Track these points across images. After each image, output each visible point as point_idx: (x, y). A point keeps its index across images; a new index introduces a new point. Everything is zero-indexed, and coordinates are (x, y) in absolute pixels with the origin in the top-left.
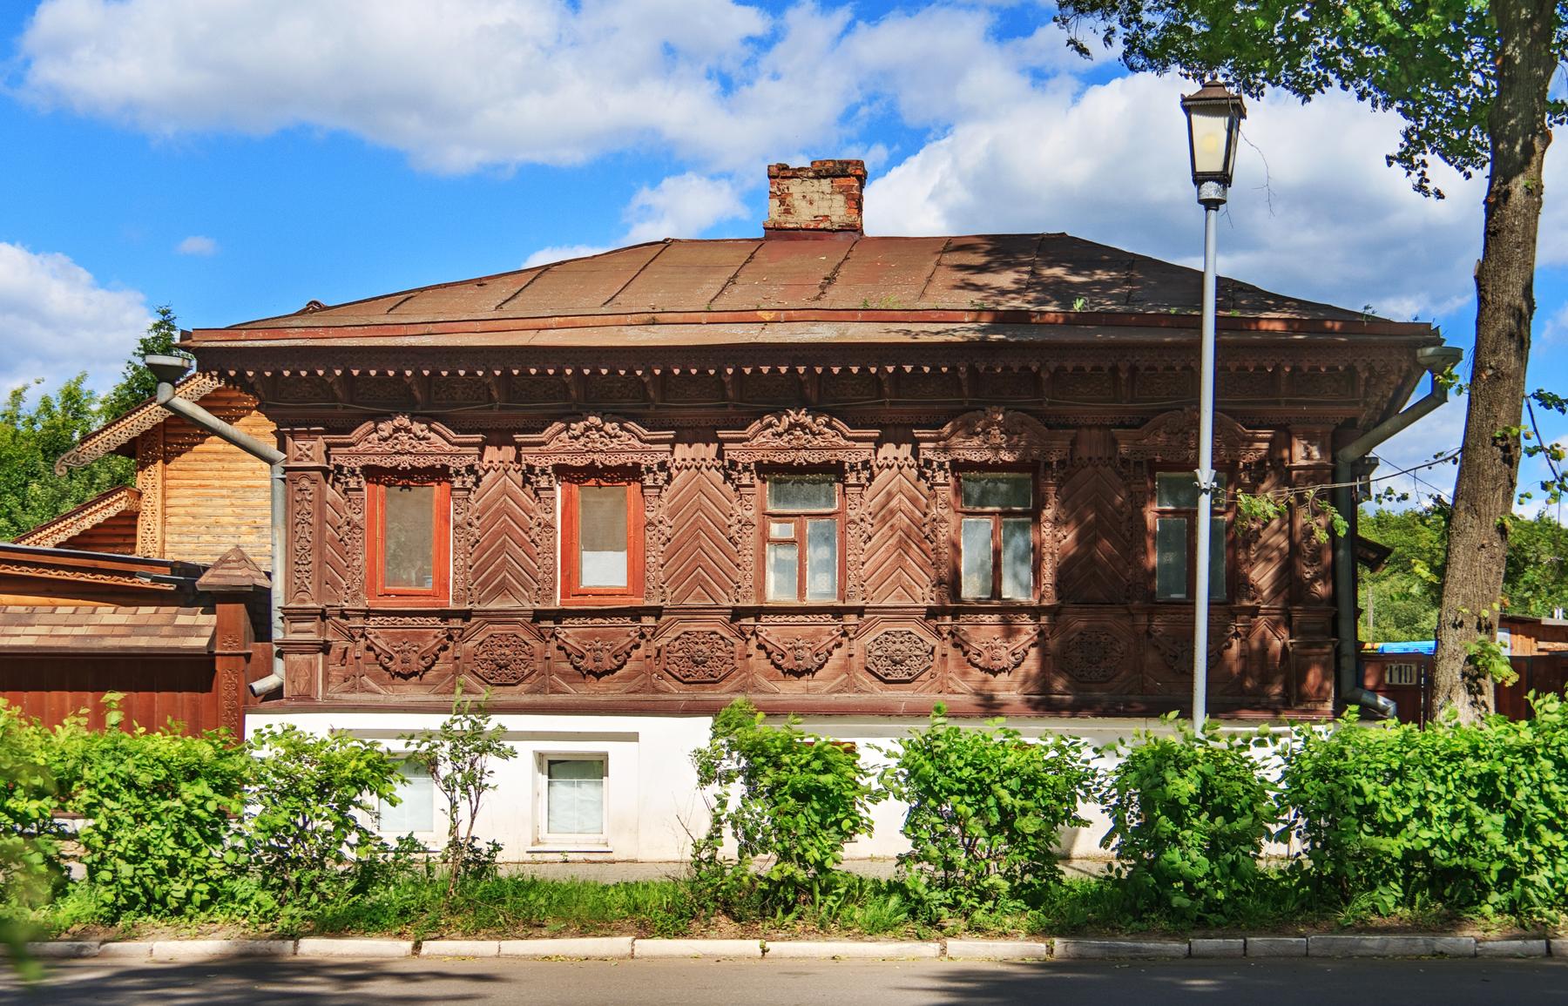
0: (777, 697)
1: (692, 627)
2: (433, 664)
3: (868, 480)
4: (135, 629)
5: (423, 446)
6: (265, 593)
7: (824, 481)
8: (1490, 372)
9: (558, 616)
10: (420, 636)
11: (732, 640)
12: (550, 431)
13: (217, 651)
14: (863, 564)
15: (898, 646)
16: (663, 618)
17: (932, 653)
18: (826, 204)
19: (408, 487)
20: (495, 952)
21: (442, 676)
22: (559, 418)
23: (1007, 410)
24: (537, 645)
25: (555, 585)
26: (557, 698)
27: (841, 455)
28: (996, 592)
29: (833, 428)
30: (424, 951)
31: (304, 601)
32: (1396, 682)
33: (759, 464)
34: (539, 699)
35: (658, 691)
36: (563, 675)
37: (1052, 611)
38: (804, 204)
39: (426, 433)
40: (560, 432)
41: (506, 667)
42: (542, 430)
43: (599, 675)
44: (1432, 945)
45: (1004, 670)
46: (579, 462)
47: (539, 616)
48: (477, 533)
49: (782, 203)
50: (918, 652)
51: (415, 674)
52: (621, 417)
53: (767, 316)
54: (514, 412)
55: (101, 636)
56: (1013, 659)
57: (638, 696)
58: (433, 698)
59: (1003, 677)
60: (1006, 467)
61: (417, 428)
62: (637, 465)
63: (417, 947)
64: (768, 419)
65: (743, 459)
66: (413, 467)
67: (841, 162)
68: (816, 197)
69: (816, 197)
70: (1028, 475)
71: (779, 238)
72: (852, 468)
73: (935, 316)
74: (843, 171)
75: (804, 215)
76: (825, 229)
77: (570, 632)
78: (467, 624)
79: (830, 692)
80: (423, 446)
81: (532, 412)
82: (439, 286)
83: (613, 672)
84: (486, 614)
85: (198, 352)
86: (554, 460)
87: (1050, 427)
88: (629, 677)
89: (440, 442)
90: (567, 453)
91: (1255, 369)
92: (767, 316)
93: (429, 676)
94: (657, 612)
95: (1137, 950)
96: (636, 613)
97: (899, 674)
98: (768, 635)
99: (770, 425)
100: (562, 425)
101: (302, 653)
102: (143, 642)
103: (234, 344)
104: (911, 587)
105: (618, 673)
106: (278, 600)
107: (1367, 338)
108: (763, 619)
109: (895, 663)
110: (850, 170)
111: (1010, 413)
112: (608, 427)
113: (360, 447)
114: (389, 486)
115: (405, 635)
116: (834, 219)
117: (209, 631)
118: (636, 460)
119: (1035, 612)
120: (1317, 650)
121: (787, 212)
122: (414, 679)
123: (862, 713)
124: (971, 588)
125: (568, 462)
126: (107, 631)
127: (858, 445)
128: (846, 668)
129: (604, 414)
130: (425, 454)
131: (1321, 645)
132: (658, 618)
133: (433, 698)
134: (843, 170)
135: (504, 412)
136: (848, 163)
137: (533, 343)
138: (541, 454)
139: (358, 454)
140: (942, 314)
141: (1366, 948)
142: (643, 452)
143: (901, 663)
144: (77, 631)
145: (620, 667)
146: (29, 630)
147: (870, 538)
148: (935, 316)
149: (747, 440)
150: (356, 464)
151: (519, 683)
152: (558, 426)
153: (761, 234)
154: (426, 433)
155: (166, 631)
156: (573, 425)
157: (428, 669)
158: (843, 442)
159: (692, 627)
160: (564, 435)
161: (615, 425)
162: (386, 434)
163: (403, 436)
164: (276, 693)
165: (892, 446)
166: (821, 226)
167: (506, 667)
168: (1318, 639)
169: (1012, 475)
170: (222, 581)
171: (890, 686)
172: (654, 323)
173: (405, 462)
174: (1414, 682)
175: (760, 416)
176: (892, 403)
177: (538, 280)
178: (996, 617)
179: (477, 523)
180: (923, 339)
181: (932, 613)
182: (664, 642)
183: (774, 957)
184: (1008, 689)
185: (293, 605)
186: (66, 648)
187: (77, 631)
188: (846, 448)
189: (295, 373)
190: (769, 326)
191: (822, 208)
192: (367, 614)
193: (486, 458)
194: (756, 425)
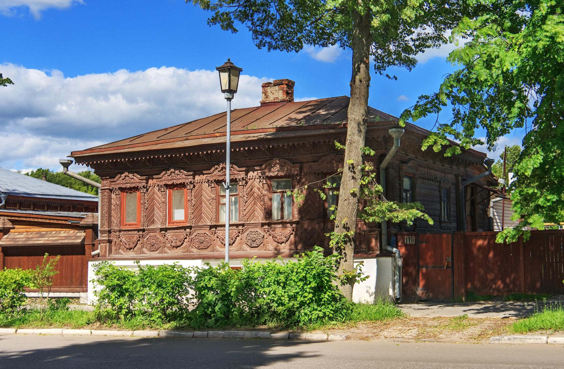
0: (221, 253)
1: (200, 232)
2: (136, 245)
3: (245, 183)
4: (67, 237)
5: (132, 181)
6: (97, 226)
7: (235, 185)
8: (349, 141)
9: (166, 230)
10: (133, 237)
11: (210, 235)
12: (162, 174)
13: (85, 243)
14: (245, 210)
15: (253, 236)
16: (193, 229)
17: (263, 237)
18: (277, 94)
19: (131, 193)
20: (32, 333)
21: (139, 249)
22: (164, 170)
23: (280, 159)
24: (161, 238)
25: (166, 220)
26: (165, 255)
27: (236, 176)
28: (282, 217)
29: (233, 168)
30: (18, 332)
31: (105, 228)
32: (408, 243)
33: (215, 180)
34: (161, 255)
35: (191, 252)
36: (168, 248)
37: (297, 223)
38: (271, 94)
39: (133, 177)
40: (165, 174)
41: (153, 246)
42: (159, 174)
43: (177, 247)
44: (257, 335)
45: (283, 242)
46: (170, 183)
47: (162, 230)
48: (147, 205)
49: (265, 95)
50: (260, 238)
51: (131, 248)
52: (179, 168)
53: (218, 135)
54: (153, 169)
55: (58, 240)
56: (285, 239)
57: (186, 254)
58: (135, 255)
59: (283, 244)
60: (281, 177)
61: (131, 175)
62: (184, 183)
63: (16, 331)
64: (216, 166)
65: (211, 179)
66: (130, 187)
67: (281, 80)
68: (274, 92)
69: (274, 92)
70: (290, 179)
71: (265, 106)
72: (239, 180)
73: (261, 131)
74: (281, 83)
75: (271, 98)
76: (276, 102)
77: (169, 234)
78: (144, 233)
79: (236, 251)
80: (132, 181)
81: (158, 169)
82: (154, 132)
83: (180, 246)
84: (148, 230)
85: (75, 158)
86: (164, 183)
87: (293, 163)
88: (184, 248)
89: (137, 179)
90: (121, 184)
91: (323, 142)
92: (218, 135)
93: (136, 248)
94: (190, 228)
95: (180, 335)
96: (185, 228)
97: (254, 245)
98: (219, 233)
99: (217, 169)
100: (165, 172)
101: (104, 243)
102: (66, 241)
103: (82, 155)
104: (258, 216)
105: (182, 246)
106: (99, 228)
107: (378, 127)
108: (168, 231)
109: (253, 241)
110: (283, 82)
111: (281, 160)
112: (176, 172)
113: (118, 182)
114: (127, 193)
115: (129, 237)
116: (280, 98)
117: (83, 238)
118: (236, 177)
119: (291, 223)
120: (373, 233)
121: (267, 97)
122: (132, 250)
123: (240, 257)
124: (276, 215)
125: (167, 183)
126: (60, 238)
127: (241, 173)
128: (240, 243)
129: (280, 159)
130: (133, 183)
131: (374, 231)
132: (191, 229)
133: (135, 255)
134: (281, 83)
135: (151, 169)
136: (283, 80)
137: (150, 149)
138: (160, 181)
139: (117, 184)
140: (262, 130)
141: (239, 335)
142: (186, 179)
143: (254, 241)
144: (54, 239)
145: (182, 245)
146: (44, 239)
147: (247, 202)
148: (261, 131)
149: (211, 173)
150: (117, 187)
151: (157, 250)
152: (164, 172)
153: (259, 105)
154: (133, 177)
155: (73, 238)
156: (168, 172)
157: (135, 247)
158: (236, 172)
159: (200, 232)
160: (166, 175)
161: (178, 171)
162: (169, 174)
163: (127, 178)
164: (98, 255)
165: (252, 172)
166: (276, 101)
167: (254, 241)
168: (374, 229)
169: (287, 179)
170: (85, 223)
171: (252, 248)
172: (187, 139)
173: (128, 186)
174: (414, 243)
175: (214, 166)
176: (249, 159)
177: (214, 122)
178: (281, 226)
179: (147, 203)
180: (249, 139)
181: (263, 225)
182: (193, 236)
183: (93, 335)
184: (285, 248)
185: (102, 229)
186: (49, 244)
187: (54, 239)
188: (237, 174)
189: (254, 148)
190: (218, 138)
191: (276, 95)
192: (120, 231)
193: (196, 179)
194: (213, 169)
